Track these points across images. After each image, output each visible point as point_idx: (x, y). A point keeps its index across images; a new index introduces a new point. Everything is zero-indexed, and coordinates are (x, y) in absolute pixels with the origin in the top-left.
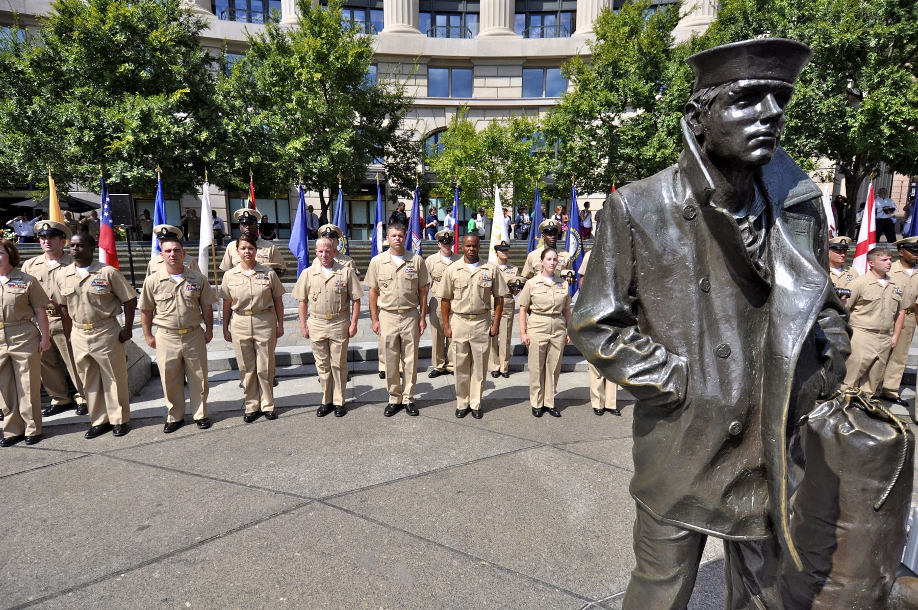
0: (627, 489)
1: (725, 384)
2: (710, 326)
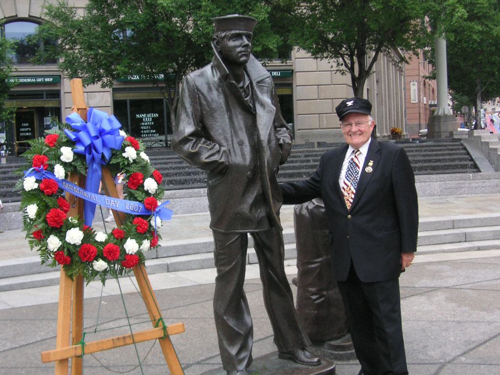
0: (209, 227)
1: (243, 155)
2: (235, 132)
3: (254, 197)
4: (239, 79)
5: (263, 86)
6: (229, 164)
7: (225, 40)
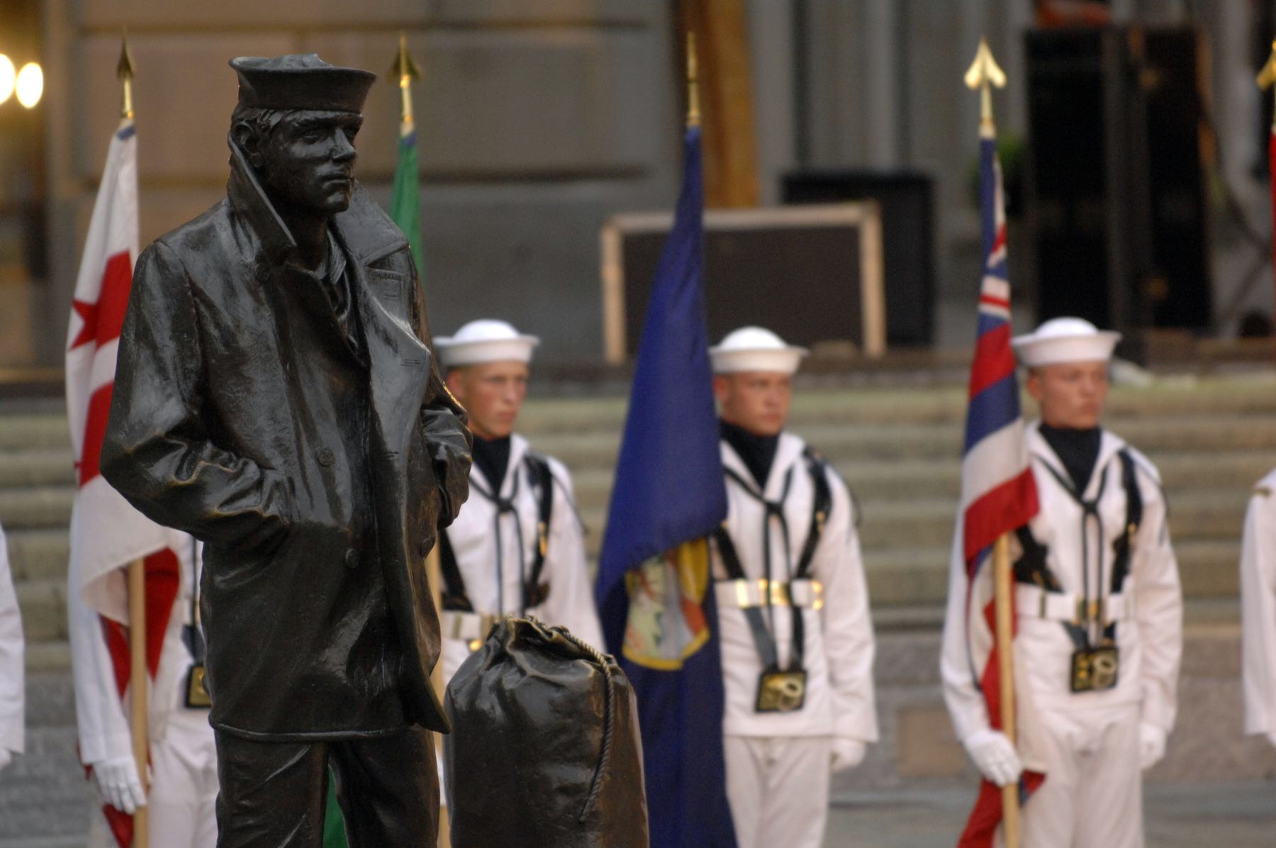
1: (334, 500)
2: (306, 426)
3: (360, 629)
4: (313, 253)
5: (387, 276)
6: (292, 524)
7: (281, 137)
